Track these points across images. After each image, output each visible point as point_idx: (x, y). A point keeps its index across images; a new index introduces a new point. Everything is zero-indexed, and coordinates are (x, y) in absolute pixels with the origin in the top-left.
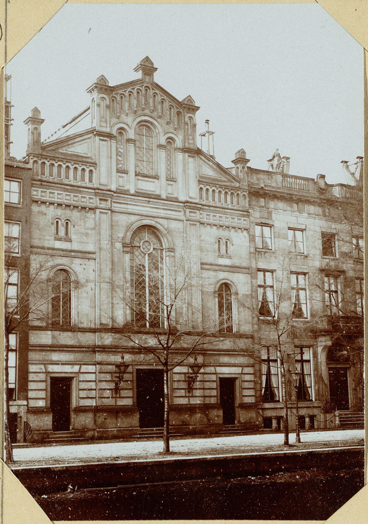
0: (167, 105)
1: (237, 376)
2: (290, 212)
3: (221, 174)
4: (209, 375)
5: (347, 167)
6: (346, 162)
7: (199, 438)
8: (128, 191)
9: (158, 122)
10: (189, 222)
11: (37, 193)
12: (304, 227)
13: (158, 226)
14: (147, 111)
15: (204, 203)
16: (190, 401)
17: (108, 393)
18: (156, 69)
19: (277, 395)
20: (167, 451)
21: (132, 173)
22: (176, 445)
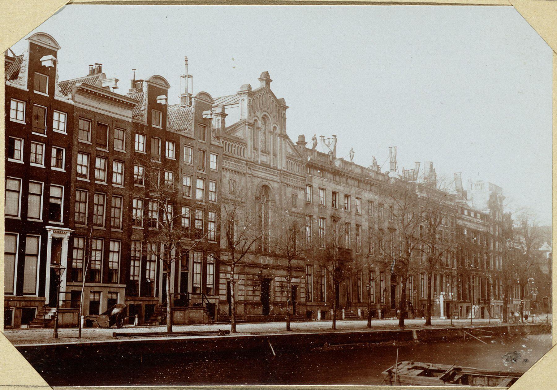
0: (274, 104)
1: (298, 284)
2: (320, 178)
3: (294, 152)
4: (197, 278)
6: (323, 137)
7: (253, 323)
9: (270, 115)
10: (282, 184)
11: (230, 164)
12: (325, 187)
13: (269, 185)
14: (268, 111)
15: (290, 172)
16: (62, 294)
17: (250, 293)
18: (272, 81)
19: (310, 297)
20: (288, 328)
21: (260, 151)
22: (293, 325)
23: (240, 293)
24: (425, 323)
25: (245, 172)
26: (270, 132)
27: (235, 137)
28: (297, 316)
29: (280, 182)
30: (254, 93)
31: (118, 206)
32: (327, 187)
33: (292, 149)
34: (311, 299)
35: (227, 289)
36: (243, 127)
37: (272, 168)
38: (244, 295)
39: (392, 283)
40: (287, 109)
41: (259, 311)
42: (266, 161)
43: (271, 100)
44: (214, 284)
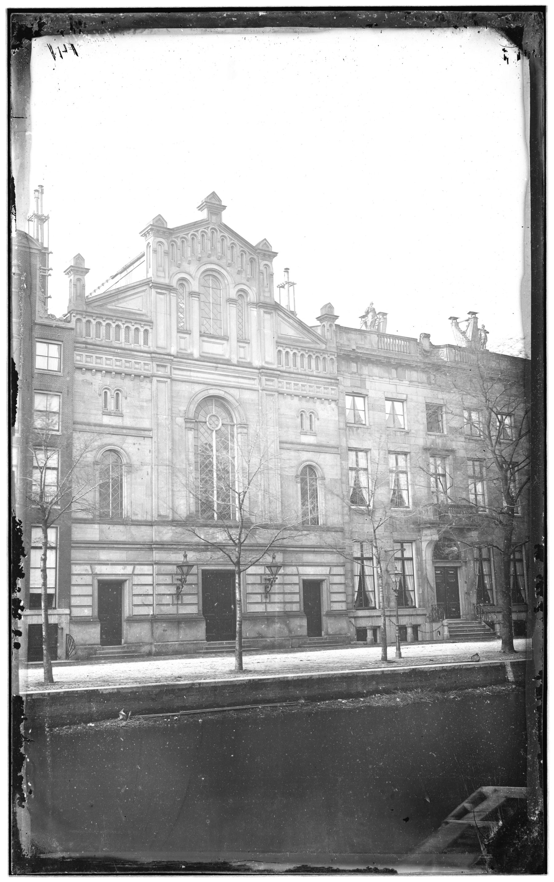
0: (237, 250)
1: (324, 578)
3: (304, 334)
5: (457, 324)
6: (455, 319)
8: (192, 354)
10: (265, 392)
12: (404, 397)
14: (213, 258)
17: (167, 600)
20: (240, 668)
24: (500, 649)
25: (149, 373)
26: (230, 301)
27: (119, 310)
28: (326, 639)
29: (260, 388)
30: (171, 232)
32: (409, 397)
33: (296, 328)
34: (373, 603)
35: (302, 593)
36: (144, 291)
37: (236, 366)
39: (437, 562)
40: (275, 260)
42: (221, 353)
43: (228, 242)
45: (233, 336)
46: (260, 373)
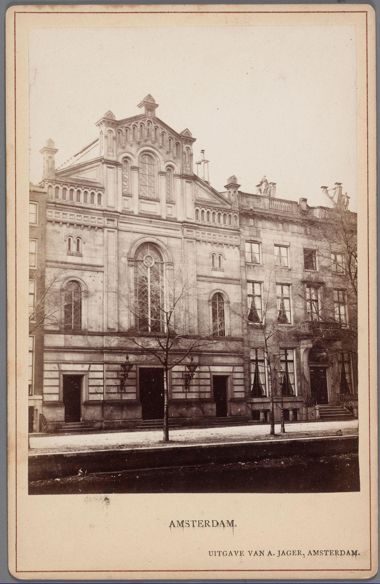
0: (167, 137)
1: (228, 374)
2: (276, 231)
5: (327, 191)
6: (326, 188)
10: (186, 240)
12: (288, 244)
18: (157, 105)
22: (175, 434)
23: (92, 390)
28: (230, 419)
29: (182, 237)
31: (314, 297)
34: (265, 393)
36: (98, 166)
38: (103, 393)
41: (211, 409)
43: (160, 131)
44: (33, 379)
45: (163, 198)
46: (183, 226)
